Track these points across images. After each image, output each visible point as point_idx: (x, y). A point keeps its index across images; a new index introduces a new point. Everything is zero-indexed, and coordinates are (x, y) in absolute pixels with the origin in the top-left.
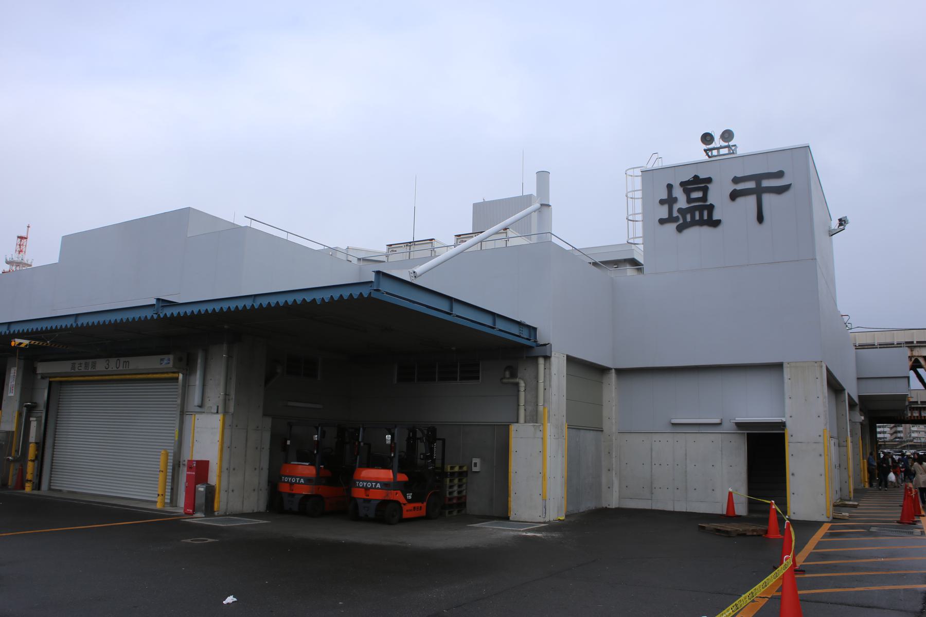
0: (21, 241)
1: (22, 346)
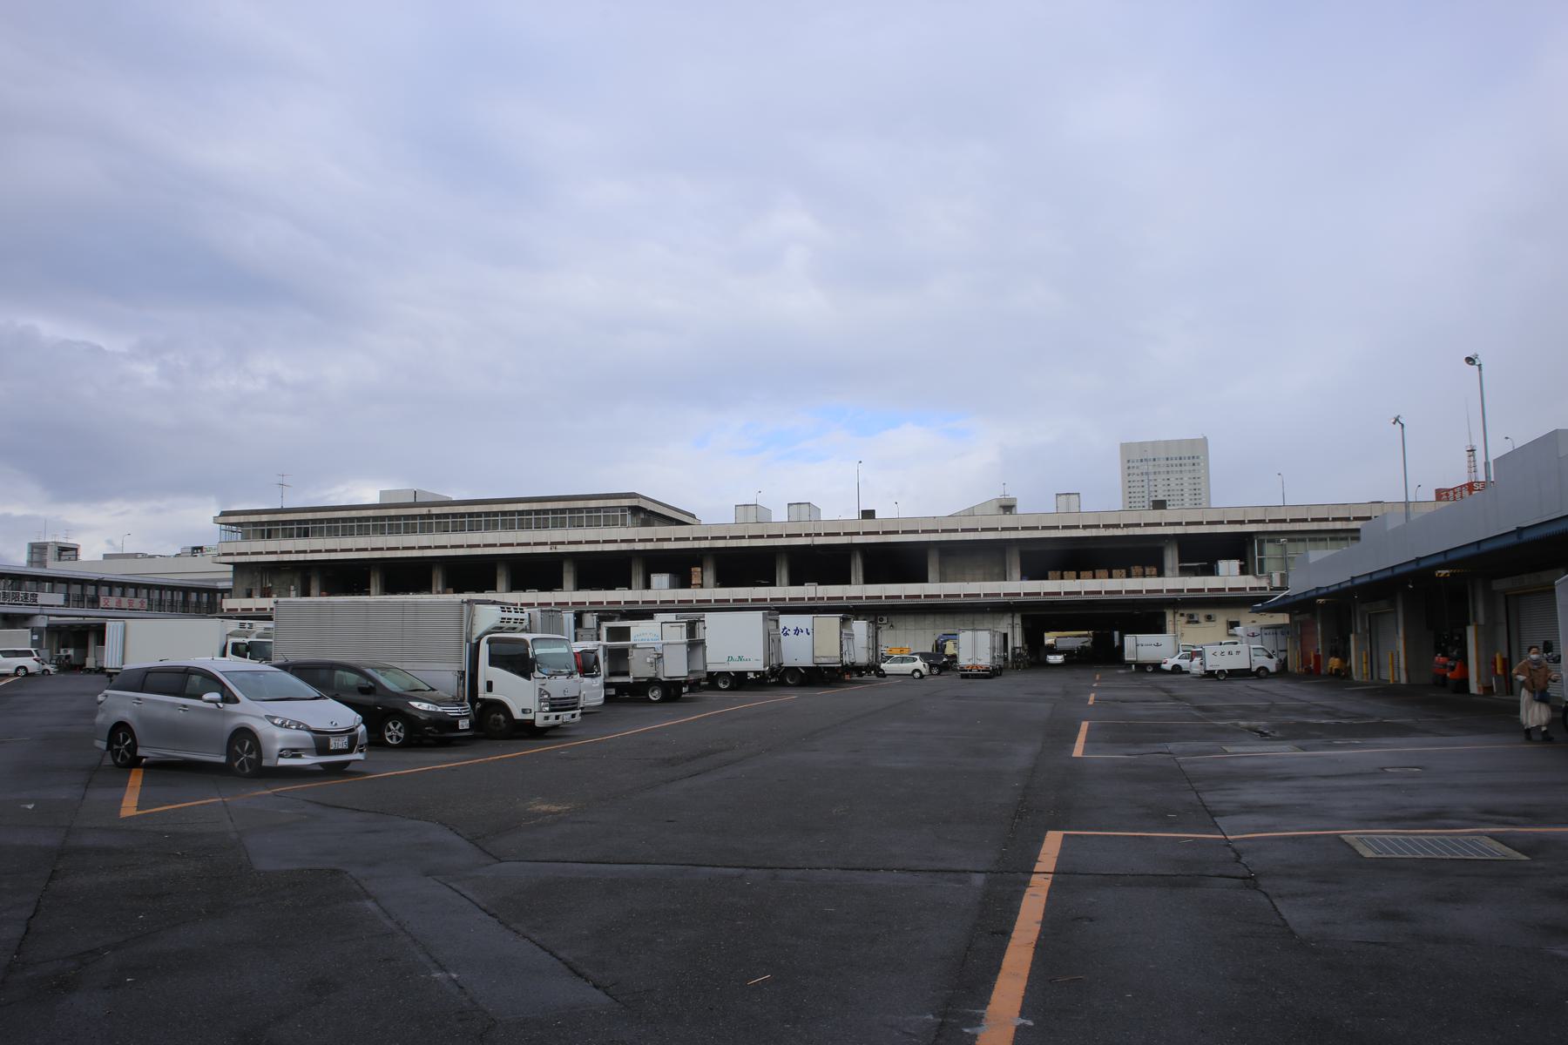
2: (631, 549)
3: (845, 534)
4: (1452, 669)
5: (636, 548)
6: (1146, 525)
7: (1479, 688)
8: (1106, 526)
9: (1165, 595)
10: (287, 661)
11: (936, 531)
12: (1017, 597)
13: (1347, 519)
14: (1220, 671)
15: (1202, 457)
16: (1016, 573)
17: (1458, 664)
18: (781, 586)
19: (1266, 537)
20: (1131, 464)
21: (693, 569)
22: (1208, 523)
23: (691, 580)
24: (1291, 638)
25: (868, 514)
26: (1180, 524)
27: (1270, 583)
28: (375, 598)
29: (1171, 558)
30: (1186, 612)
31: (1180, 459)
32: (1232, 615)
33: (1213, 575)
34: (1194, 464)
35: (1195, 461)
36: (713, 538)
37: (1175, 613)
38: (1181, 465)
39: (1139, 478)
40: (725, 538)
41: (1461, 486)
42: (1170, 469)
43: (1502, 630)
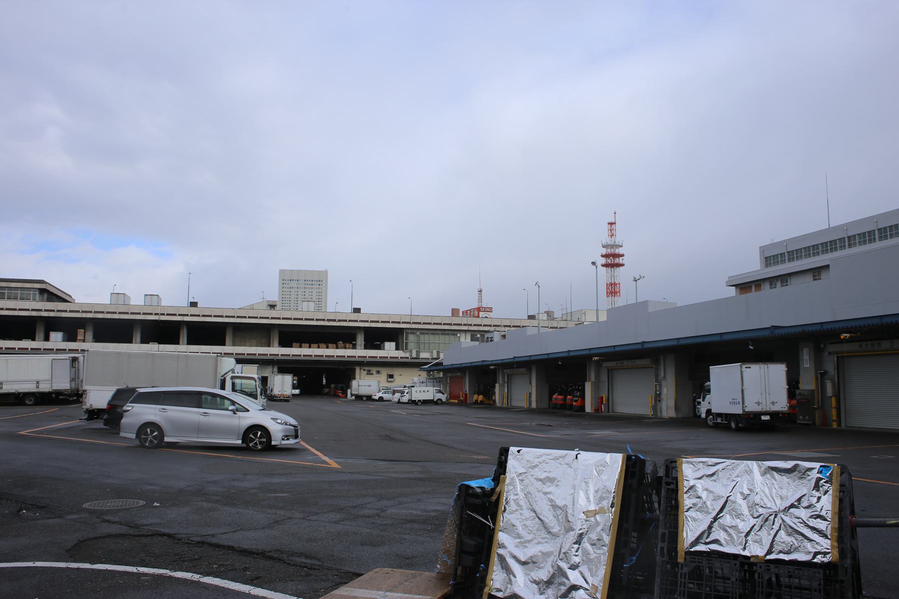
0: (611, 226)
1: (847, 338)
2: (39, 315)
3: (179, 315)
4: (576, 401)
5: (42, 315)
6: (284, 319)
7: (592, 410)
8: (329, 320)
9: (357, 359)
10: (128, 387)
11: (234, 317)
12: (243, 356)
13: (450, 324)
14: (418, 400)
15: (324, 281)
16: (276, 343)
17: (580, 399)
18: (136, 343)
19: (410, 331)
20: (284, 282)
21: (78, 330)
22: (382, 322)
23: (77, 337)
24: (443, 384)
25: (357, 310)
26: (367, 321)
27: (411, 355)
28: (183, 348)
29: (360, 340)
30: (367, 368)
31: (312, 281)
32: (390, 371)
33: (380, 349)
34: (319, 285)
35: (320, 283)
36: (95, 312)
37: (361, 369)
38: (312, 285)
39: (289, 290)
40: (103, 312)
41: (474, 309)
42: (306, 286)
43: (506, 385)
